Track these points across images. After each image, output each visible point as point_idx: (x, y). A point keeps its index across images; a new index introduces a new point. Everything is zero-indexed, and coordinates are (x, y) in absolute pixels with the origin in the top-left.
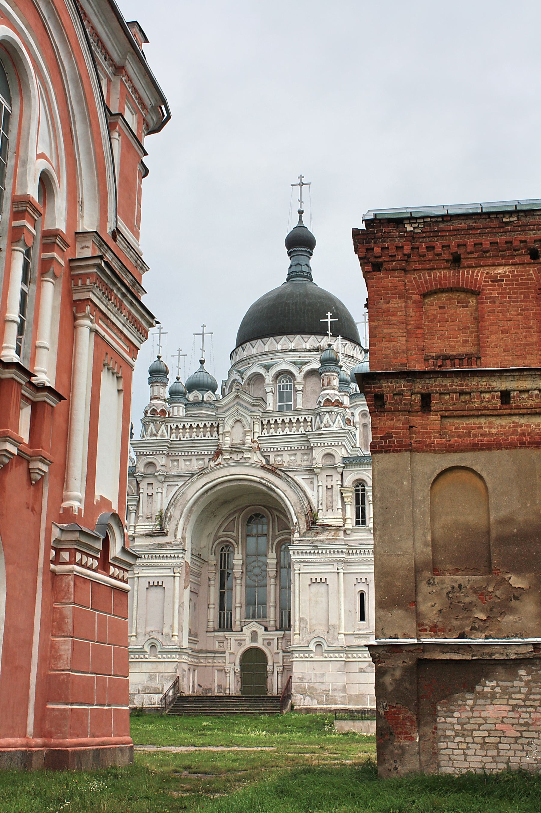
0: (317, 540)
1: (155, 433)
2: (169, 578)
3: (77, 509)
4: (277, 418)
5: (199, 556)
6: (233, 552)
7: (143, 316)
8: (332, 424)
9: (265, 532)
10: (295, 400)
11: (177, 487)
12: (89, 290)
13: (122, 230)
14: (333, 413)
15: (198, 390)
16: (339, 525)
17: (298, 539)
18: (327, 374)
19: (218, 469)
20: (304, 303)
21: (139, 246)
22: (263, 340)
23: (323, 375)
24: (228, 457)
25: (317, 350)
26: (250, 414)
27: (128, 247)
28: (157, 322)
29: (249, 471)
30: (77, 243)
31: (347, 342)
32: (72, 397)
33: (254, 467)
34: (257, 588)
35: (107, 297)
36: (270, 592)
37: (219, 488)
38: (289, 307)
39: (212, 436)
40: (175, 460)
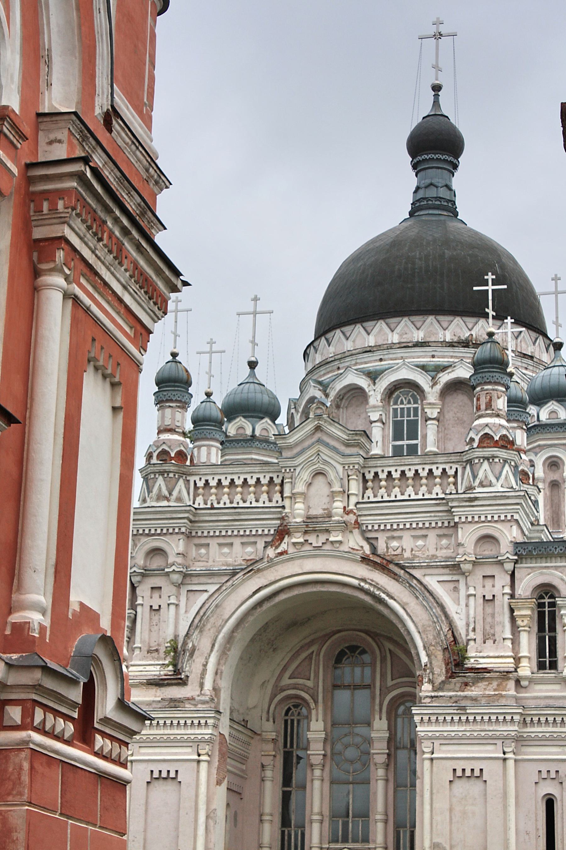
0: (466, 697)
1: (167, 494)
2: (188, 764)
3: (36, 626)
4: (392, 469)
5: (244, 724)
6: (308, 718)
7: (159, 272)
8: (494, 480)
9: (367, 681)
10: (425, 437)
11: (205, 596)
12: (63, 220)
13: (122, 110)
14: (497, 460)
15: (245, 417)
16: (506, 669)
17: (429, 694)
18: (486, 387)
19: (283, 562)
20: (442, 256)
21: (152, 141)
22: (365, 324)
23: (478, 389)
24: (301, 540)
25: (466, 344)
26: (341, 460)
27: (133, 142)
28: (185, 284)
29: (339, 566)
30: (41, 133)
31: (524, 329)
32: (30, 418)
33: (348, 559)
34: (351, 786)
35: (95, 234)
36: (375, 793)
37: (283, 597)
38: (414, 263)
39: (270, 501)
40: (202, 545)
